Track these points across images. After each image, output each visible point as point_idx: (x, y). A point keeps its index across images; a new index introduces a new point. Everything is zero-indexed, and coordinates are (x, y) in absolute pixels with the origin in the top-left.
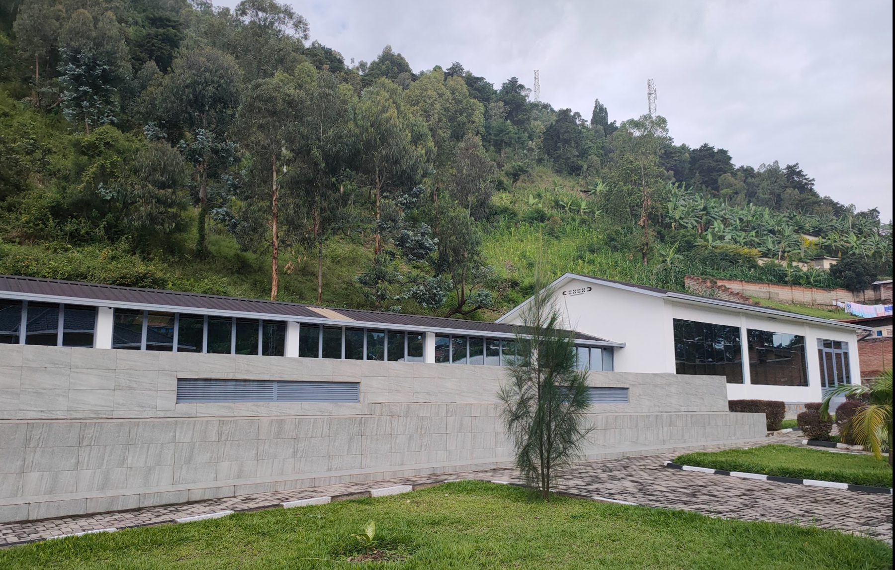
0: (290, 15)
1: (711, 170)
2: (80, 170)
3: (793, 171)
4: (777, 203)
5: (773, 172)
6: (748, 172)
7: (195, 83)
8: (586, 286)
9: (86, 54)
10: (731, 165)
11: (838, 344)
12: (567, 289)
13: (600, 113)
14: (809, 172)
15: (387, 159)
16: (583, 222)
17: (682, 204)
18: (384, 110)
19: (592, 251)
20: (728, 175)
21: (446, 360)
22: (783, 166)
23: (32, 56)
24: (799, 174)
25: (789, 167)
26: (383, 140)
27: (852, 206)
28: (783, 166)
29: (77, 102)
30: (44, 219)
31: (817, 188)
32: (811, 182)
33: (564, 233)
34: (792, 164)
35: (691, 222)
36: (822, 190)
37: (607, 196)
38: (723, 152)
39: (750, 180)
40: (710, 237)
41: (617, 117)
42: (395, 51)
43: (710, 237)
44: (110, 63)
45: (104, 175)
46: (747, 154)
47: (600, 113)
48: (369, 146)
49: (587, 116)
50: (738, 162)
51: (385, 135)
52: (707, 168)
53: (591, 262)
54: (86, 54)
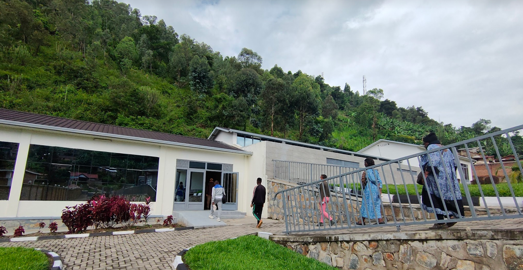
0: (256, 56)
1: (388, 109)
2: (216, 107)
3: (419, 109)
4: (414, 121)
5: (412, 110)
6: (402, 110)
7: (247, 79)
8: (387, 143)
9: (199, 69)
10: (396, 107)
11: (465, 166)
12: (379, 144)
13: (347, 88)
14: (425, 109)
15: (309, 103)
16: (349, 126)
17: (384, 120)
18: (308, 87)
19: (355, 136)
20: (396, 111)
21: (183, 200)
22: (416, 107)
23: (178, 70)
24: (422, 110)
25: (418, 108)
26: (308, 97)
27: (442, 122)
28: (416, 107)
29: (195, 85)
30: (206, 121)
31: (428, 116)
32: (427, 113)
33: (343, 129)
34: (419, 107)
35: (387, 127)
36: (430, 116)
37: (356, 117)
38: (393, 102)
39: (403, 112)
40: (396, 132)
41: (353, 89)
42: (279, 66)
43: (396, 132)
44: (205, 72)
45: (224, 108)
46: (403, 103)
47: (347, 88)
48: (303, 98)
49: (342, 88)
50: (398, 106)
51: (308, 96)
52: (388, 107)
53: (356, 140)
54: (199, 69)
